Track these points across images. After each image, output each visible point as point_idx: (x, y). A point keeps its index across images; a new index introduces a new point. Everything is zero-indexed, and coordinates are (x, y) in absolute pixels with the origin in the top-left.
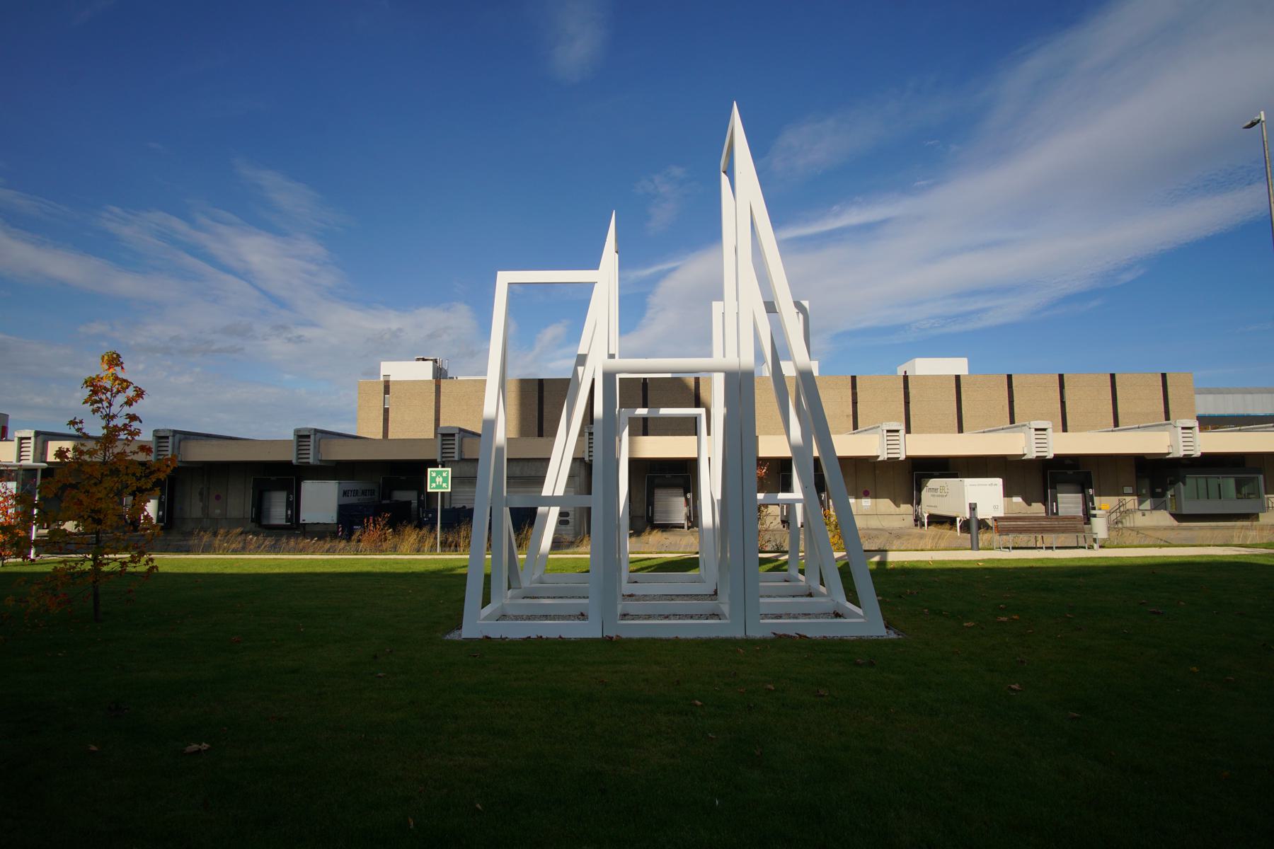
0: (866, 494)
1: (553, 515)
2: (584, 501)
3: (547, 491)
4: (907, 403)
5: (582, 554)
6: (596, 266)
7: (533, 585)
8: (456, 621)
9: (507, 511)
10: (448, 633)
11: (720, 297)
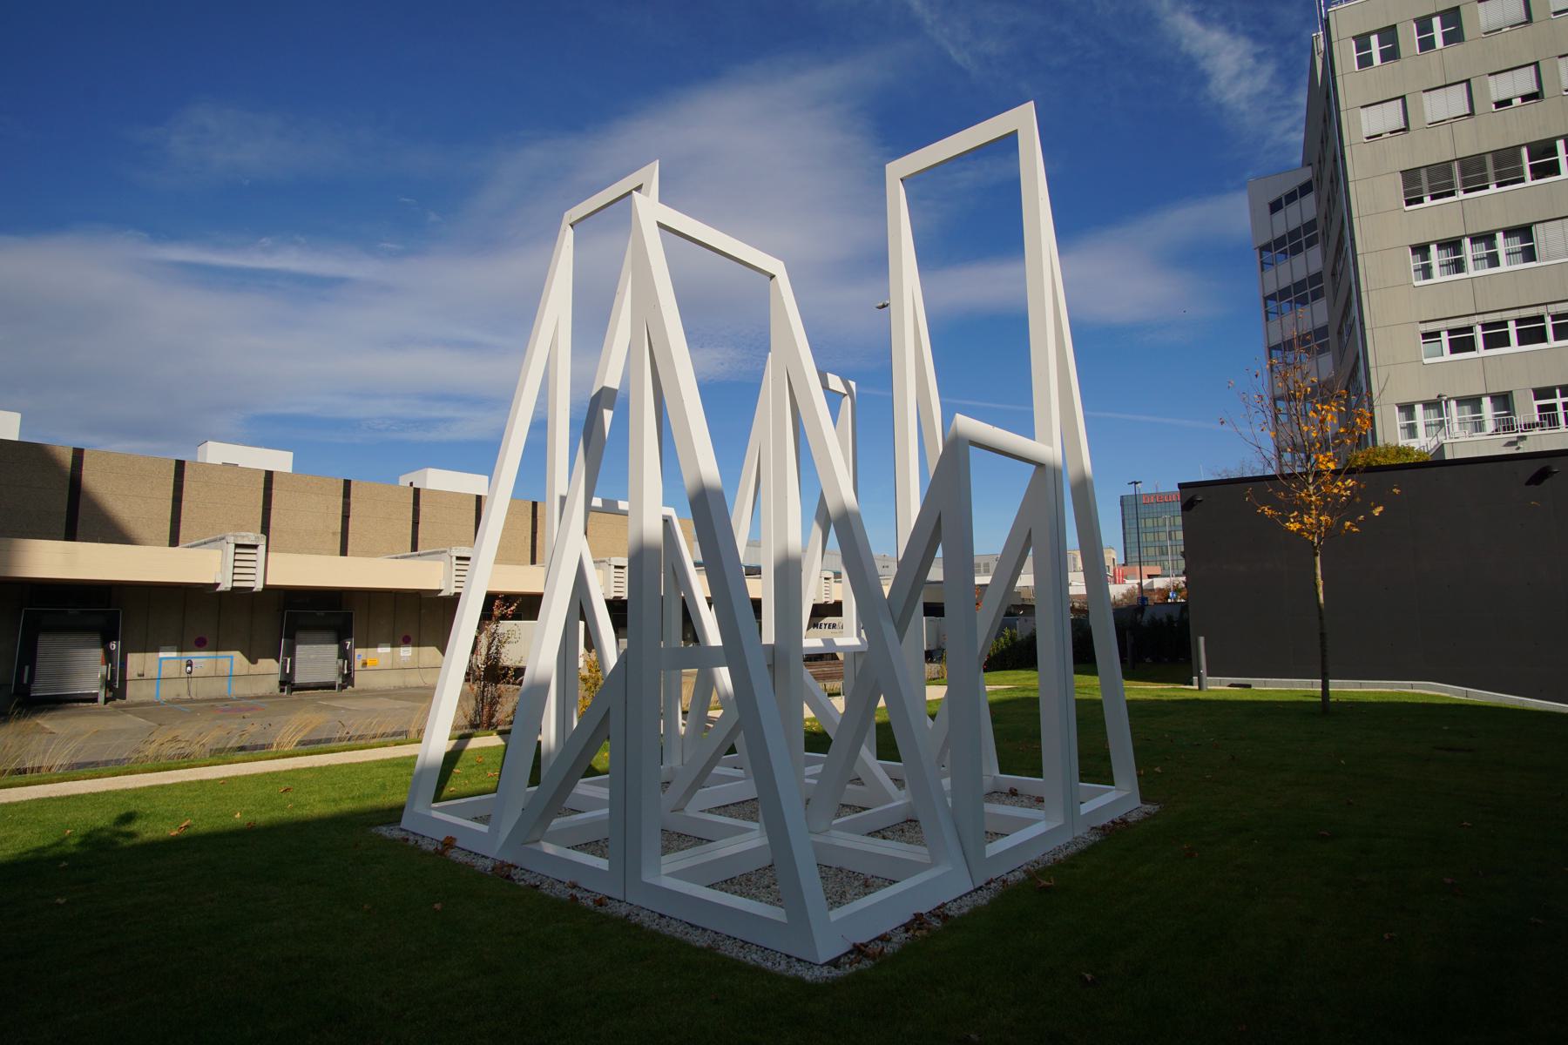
0: (406, 641)
4: (416, 524)
7: (148, 831)
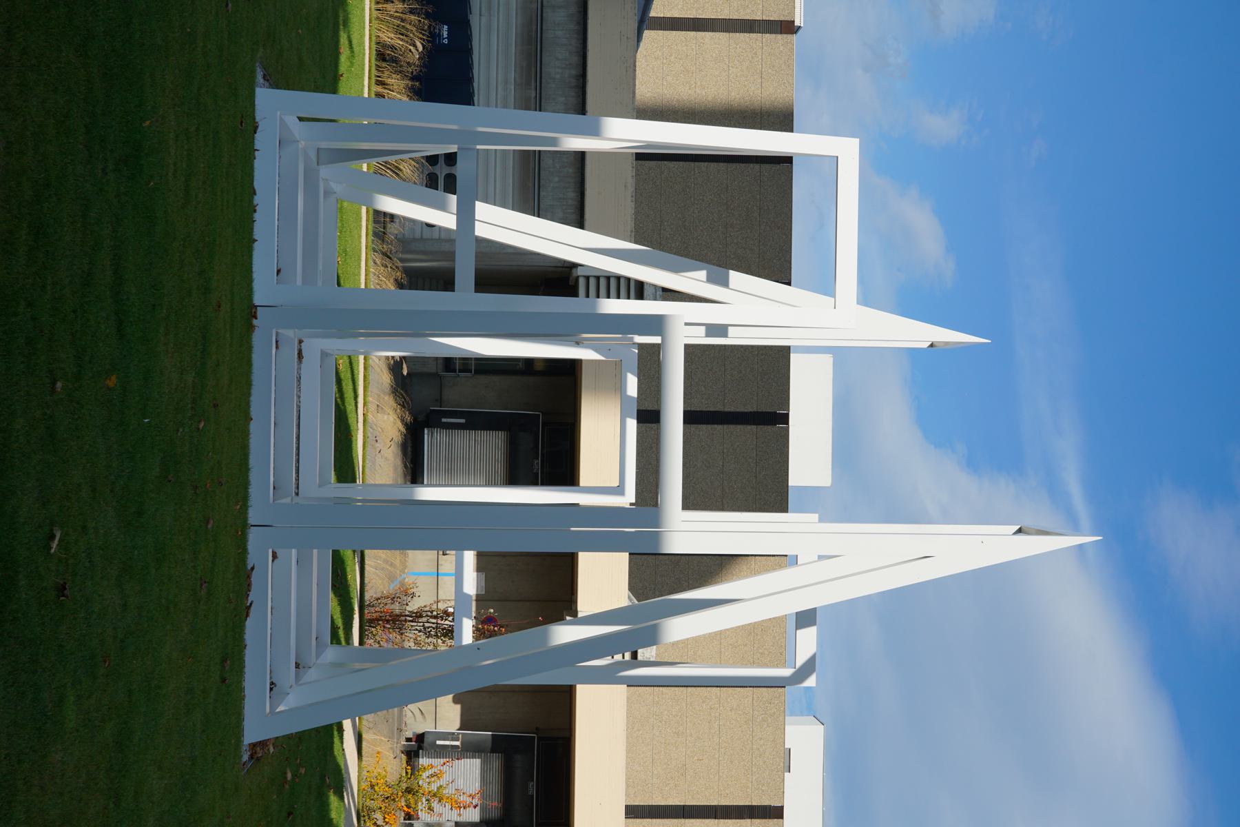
1: (441, 217)
2: (465, 274)
3: (483, 210)
5: (367, 273)
6: (867, 298)
8: (279, 81)
9: (453, 148)
10: (264, 68)
11: (821, 521)
